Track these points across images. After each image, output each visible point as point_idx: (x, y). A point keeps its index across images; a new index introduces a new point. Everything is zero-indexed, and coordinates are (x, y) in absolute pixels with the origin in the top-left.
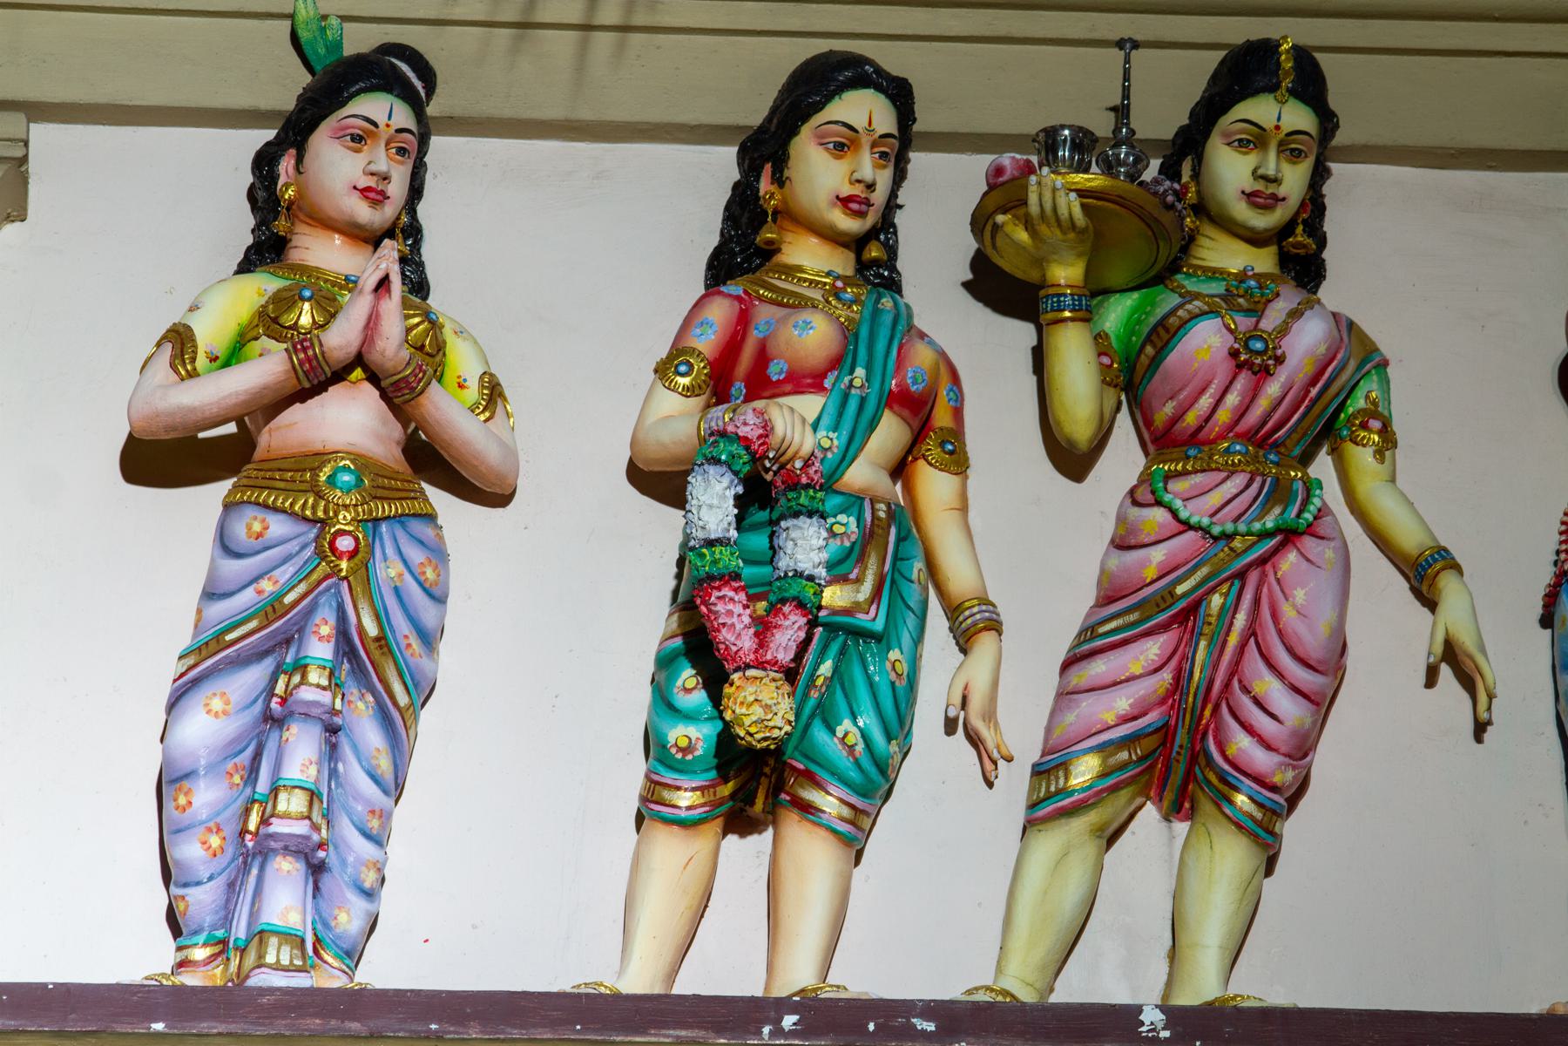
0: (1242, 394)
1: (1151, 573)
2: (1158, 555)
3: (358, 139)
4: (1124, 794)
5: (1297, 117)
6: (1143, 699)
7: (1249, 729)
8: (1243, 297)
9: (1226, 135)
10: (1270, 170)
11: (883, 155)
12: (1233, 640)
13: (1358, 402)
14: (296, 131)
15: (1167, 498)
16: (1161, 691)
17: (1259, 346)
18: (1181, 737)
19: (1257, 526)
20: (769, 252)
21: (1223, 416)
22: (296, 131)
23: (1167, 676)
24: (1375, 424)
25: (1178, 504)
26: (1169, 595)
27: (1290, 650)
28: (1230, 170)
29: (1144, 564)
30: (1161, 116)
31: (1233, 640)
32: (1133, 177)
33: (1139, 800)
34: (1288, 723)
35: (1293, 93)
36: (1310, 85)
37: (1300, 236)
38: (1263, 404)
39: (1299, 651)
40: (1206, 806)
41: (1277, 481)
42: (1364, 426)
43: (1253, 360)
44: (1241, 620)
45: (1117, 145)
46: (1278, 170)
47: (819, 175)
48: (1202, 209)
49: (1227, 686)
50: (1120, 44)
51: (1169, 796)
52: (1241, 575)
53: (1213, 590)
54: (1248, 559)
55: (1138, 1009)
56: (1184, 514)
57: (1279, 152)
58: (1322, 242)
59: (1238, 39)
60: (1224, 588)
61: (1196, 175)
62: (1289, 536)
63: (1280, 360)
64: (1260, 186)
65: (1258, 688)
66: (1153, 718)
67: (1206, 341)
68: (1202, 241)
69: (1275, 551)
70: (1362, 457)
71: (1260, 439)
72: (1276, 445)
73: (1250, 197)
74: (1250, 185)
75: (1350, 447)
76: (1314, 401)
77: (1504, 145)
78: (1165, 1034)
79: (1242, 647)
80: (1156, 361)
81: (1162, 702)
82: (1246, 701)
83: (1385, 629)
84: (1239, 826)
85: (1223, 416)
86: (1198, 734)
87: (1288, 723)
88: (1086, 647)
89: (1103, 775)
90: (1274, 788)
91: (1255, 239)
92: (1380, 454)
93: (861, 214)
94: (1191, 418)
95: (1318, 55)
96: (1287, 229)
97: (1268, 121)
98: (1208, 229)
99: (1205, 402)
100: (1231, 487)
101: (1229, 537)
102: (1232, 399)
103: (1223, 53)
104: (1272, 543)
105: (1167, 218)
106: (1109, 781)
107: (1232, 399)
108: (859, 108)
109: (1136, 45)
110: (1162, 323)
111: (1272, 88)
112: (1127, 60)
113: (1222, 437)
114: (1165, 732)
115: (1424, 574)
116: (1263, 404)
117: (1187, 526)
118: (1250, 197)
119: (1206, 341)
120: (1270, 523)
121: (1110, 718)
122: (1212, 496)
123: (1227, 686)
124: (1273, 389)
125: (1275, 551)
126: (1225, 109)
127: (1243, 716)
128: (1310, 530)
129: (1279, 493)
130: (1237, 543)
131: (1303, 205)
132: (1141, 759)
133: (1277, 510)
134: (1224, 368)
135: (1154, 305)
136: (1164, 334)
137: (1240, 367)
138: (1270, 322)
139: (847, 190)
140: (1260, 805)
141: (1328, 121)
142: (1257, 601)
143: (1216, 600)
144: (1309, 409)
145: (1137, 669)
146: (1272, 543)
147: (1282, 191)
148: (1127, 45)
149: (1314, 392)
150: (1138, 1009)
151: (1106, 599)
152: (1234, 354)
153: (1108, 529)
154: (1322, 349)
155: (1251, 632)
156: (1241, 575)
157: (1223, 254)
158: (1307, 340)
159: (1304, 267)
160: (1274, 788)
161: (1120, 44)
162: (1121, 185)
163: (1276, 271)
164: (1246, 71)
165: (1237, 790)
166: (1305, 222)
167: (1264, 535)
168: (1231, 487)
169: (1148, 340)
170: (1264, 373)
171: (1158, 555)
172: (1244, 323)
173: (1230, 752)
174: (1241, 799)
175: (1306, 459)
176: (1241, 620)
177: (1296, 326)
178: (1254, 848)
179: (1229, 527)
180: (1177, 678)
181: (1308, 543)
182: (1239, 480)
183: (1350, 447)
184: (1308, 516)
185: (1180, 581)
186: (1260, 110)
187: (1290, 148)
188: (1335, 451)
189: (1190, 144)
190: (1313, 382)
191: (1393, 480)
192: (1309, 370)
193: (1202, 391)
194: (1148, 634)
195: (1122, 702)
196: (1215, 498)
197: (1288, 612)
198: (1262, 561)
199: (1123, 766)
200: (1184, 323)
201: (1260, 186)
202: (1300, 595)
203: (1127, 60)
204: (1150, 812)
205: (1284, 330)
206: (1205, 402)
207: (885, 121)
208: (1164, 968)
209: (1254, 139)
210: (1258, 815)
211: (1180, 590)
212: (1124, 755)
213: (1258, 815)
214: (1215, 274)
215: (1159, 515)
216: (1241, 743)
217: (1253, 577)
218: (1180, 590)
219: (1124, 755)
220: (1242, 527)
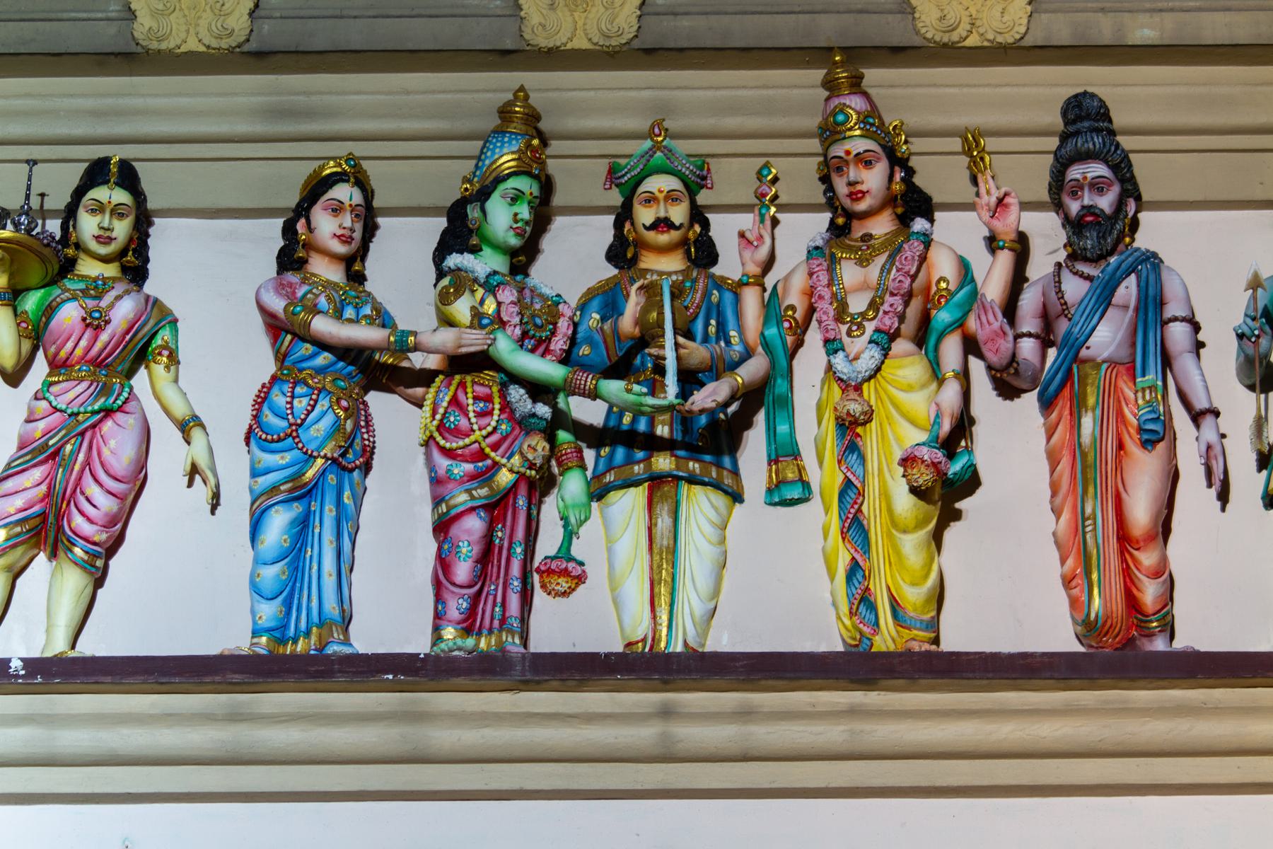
0: (89, 341)
1: (38, 435)
2: (41, 425)
3: (334, 210)
4: (20, 550)
5: (121, 196)
6: (30, 500)
7: (82, 513)
8: (97, 288)
9: (85, 207)
10: (106, 224)
11: (357, 216)
12: (77, 467)
13: (158, 341)
14: (303, 209)
15: (47, 395)
16: (41, 496)
17: (97, 315)
18: (51, 519)
19: (90, 409)
20: (303, 262)
21: (79, 352)
22: (303, 209)
23: (44, 488)
24: (166, 353)
25: (52, 398)
26: (45, 446)
27: (107, 472)
28: (88, 225)
29: (35, 430)
30: (59, 200)
31: (77, 467)
32: (29, 231)
33: (36, 551)
34: (103, 510)
35: (117, 184)
36: (128, 177)
37: (130, 257)
38: (99, 345)
39: (112, 472)
40: (61, 553)
41: (105, 384)
42: (160, 354)
43: (95, 323)
44: (81, 457)
45: (20, 215)
46: (110, 223)
47: (326, 226)
48: (78, 246)
49: (74, 491)
50: (27, 162)
51: (49, 549)
52: (82, 434)
53: (67, 442)
54: (85, 428)
55: (9, 660)
56: (54, 404)
57: (111, 214)
58: (147, 260)
59: (96, 157)
60: (73, 441)
61: (74, 227)
62: (108, 413)
63: (108, 322)
64: (101, 233)
65: (88, 492)
66: (37, 509)
67: (70, 314)
68: (80, 261)
69: (101, 421)
70: (159, 370)
71: (98, 363)
72: (107, 366)
73: (97, 238)
74: (97, 232)
75: (153, 365)
76: (128, 343)
77: (240, 206)
78: (23, 672)
79: (82, 471)
80: (47, 324)
81: (42, 500)
82: (82, 500)
83: (168, 455)
84: (76, 564)
85: (79, 352)
86: (59, 517)
87: (103, 510)
88: (10, 471)
89: (7, 540)
90: (95, 544)
91: (105, 260)
92: (167, 368)
93: (349, 243)
94: (63, 354)
95: (134, 164)
96: (123, 253)
97: (105, 200)
98: (82, 255)
99: (70, 345)
100: (80, 389)
101: (77, 414)
102: (83, 343)
103: (86, 165)
104: (97, 417)
105: (46, 251)
106: (11, 543)
107: (83, 343)
108: (345, 193)
109: (35, 162)
110: (49, 305)
111: (106, 182)
112: (31, 170)
113: (78, 363)
114: (43, 516)
115: (188, 426)
116: (99, 345)
117: (56, 410)
118: (97, 238)
119: (70, 314)
120: (96, 407)
121: (12, 511)
122: (72, 394)
123: (74, 491)
124: (104, 337)
125: (101, 421)
126: (84, 194)
127: (80, 507)
128: (120, 409)
129: (105, 390)
130: (80, 418)
131: (131, 240)
132: (28, 531)
133: (103, 400)
134: (79, 327)
135: (50, 295)
136: (49, 310)
137: (88, 326)
138: (104, 303)
139: (339, 232)
140: (86, 552)
141: (368, 194)
142: (90, 447)
143: (68, 448)
144: (125, 347)
145: (28, 484)
146: (97, 417)
147: (114, 235)
148: (33, 163)
149: (128, 337)
150: (9, 660)
151: (20, 448)
152: (84, 319)
153: (24, 415)
154: (131, 316)
155: (88, 463)
156: (82, 434)
157: (88, 268)
158: (124, 310)
159: (136, 273)
160: (95, 544)
161: (27, 162)
162: (21, 236)
163: (119, 275)
164: (96, 173)
165: (74, 545)
166: (134, 251)
167: (94, 413)
168: (80, 389)
169: (43, 314)
170: (98, 329)
171: (41, 425)
172: (91, 303)
173: (73, 525)
174: (77, 550)
175: (130, 374)
176: (81, 457)
177: (118, 304)
178: (85, 575)
179: (75, 410)
180: (49, 488)
181: (119, 416)
182: (85, 385)
183: (153, 365)
184: (119, 402)
185: (51, 438)
186: (100, 193)
187: (117, 212)
188: (147, 367)
189: (70, 214)
190: (127, 332)
191: (176, 381)
192: (124, 326)
193: (68, 339)
194: (35, 466)
195: (19, 502)
196: (71, 395)
197: (106, 452)
198: (94, 426)
199: (18, 535)
200: (59, 304)
201: (101, 233)
202: (112, 443)
203: (31, 170)
204: (42, 558)
205: (112, 306)
206: (70, 345)
207: (358, 198)
208: (44, 637)
209: (99, 209)
210: (86, 558)
211: (51, 443)
212: (18, 529)
213: (86, 558)
214: (83, 278)
215: (44, 404)
216: (78, 520)
217: (88, 435)
218: (51, 443)
219: (18, 529)
220: (82, 409)
